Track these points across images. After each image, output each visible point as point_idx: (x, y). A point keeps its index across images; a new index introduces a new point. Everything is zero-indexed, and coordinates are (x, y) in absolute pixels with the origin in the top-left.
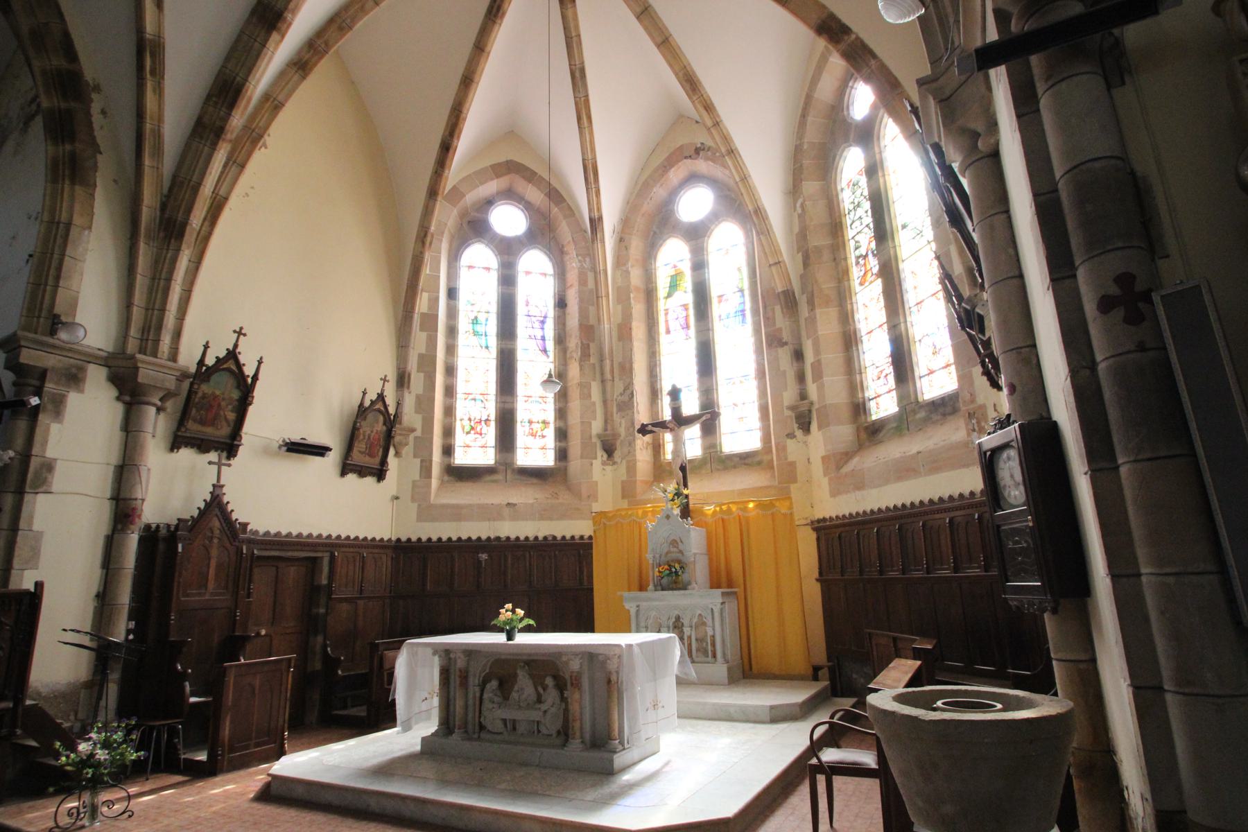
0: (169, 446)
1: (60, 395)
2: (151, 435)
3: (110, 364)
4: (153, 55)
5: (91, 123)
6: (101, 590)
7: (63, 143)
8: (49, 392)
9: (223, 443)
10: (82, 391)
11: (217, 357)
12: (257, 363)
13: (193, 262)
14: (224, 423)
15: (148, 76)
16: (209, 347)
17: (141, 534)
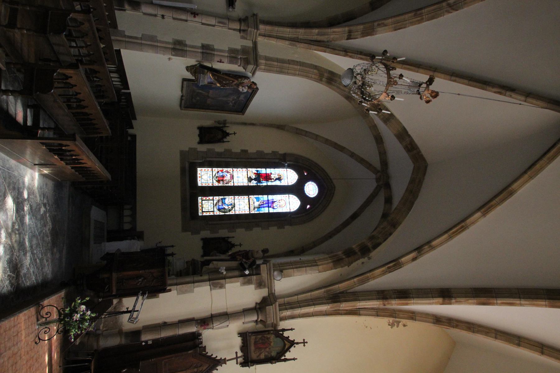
0: (240, 332)
1: (252, 282)
2: (244, 321)
3: (270, 295)
4: (394, 265)
5: (357, 260)
6: (168, 323)
7: (344, 255)
8: (252, 278)
9: (248, 357)
10: (256, 289)
11: (289, 337)
12: (293, 358)
13: (326, 313)
14: (258, 354)
15: (387, 267)
16: (292, 330)
17: (196, 332)
